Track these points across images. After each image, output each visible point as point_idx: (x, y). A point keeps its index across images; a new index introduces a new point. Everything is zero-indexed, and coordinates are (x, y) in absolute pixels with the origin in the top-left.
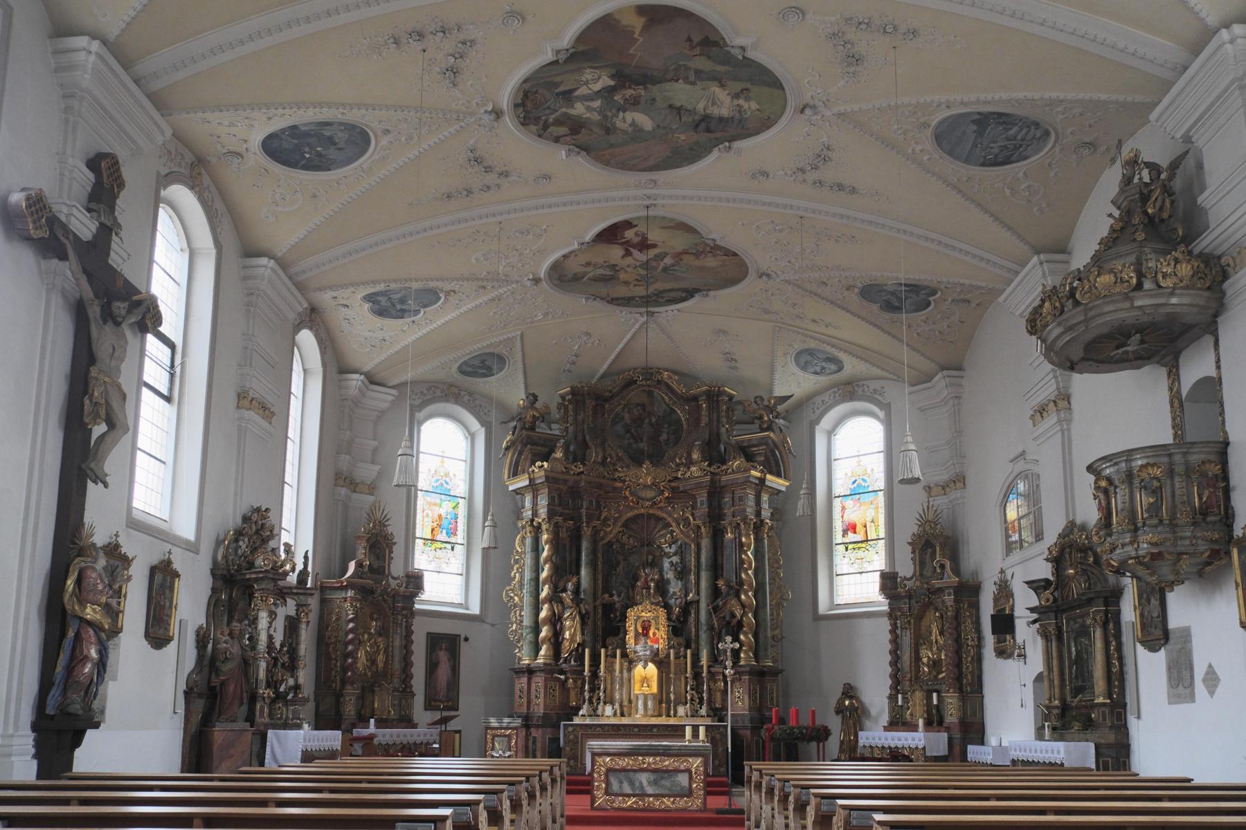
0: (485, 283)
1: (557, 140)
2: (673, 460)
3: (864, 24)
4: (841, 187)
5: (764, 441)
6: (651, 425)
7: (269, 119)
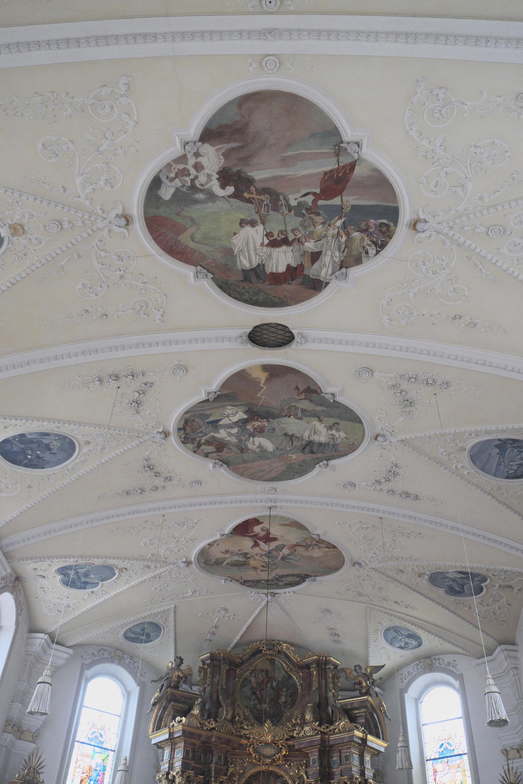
0: (149, 563)
1: (206, 455)
2: (290, 720)
3: (413, 379)
4: (407, 495)
5: (363, 705)
6: (273, 688)
7: (6, 427)
